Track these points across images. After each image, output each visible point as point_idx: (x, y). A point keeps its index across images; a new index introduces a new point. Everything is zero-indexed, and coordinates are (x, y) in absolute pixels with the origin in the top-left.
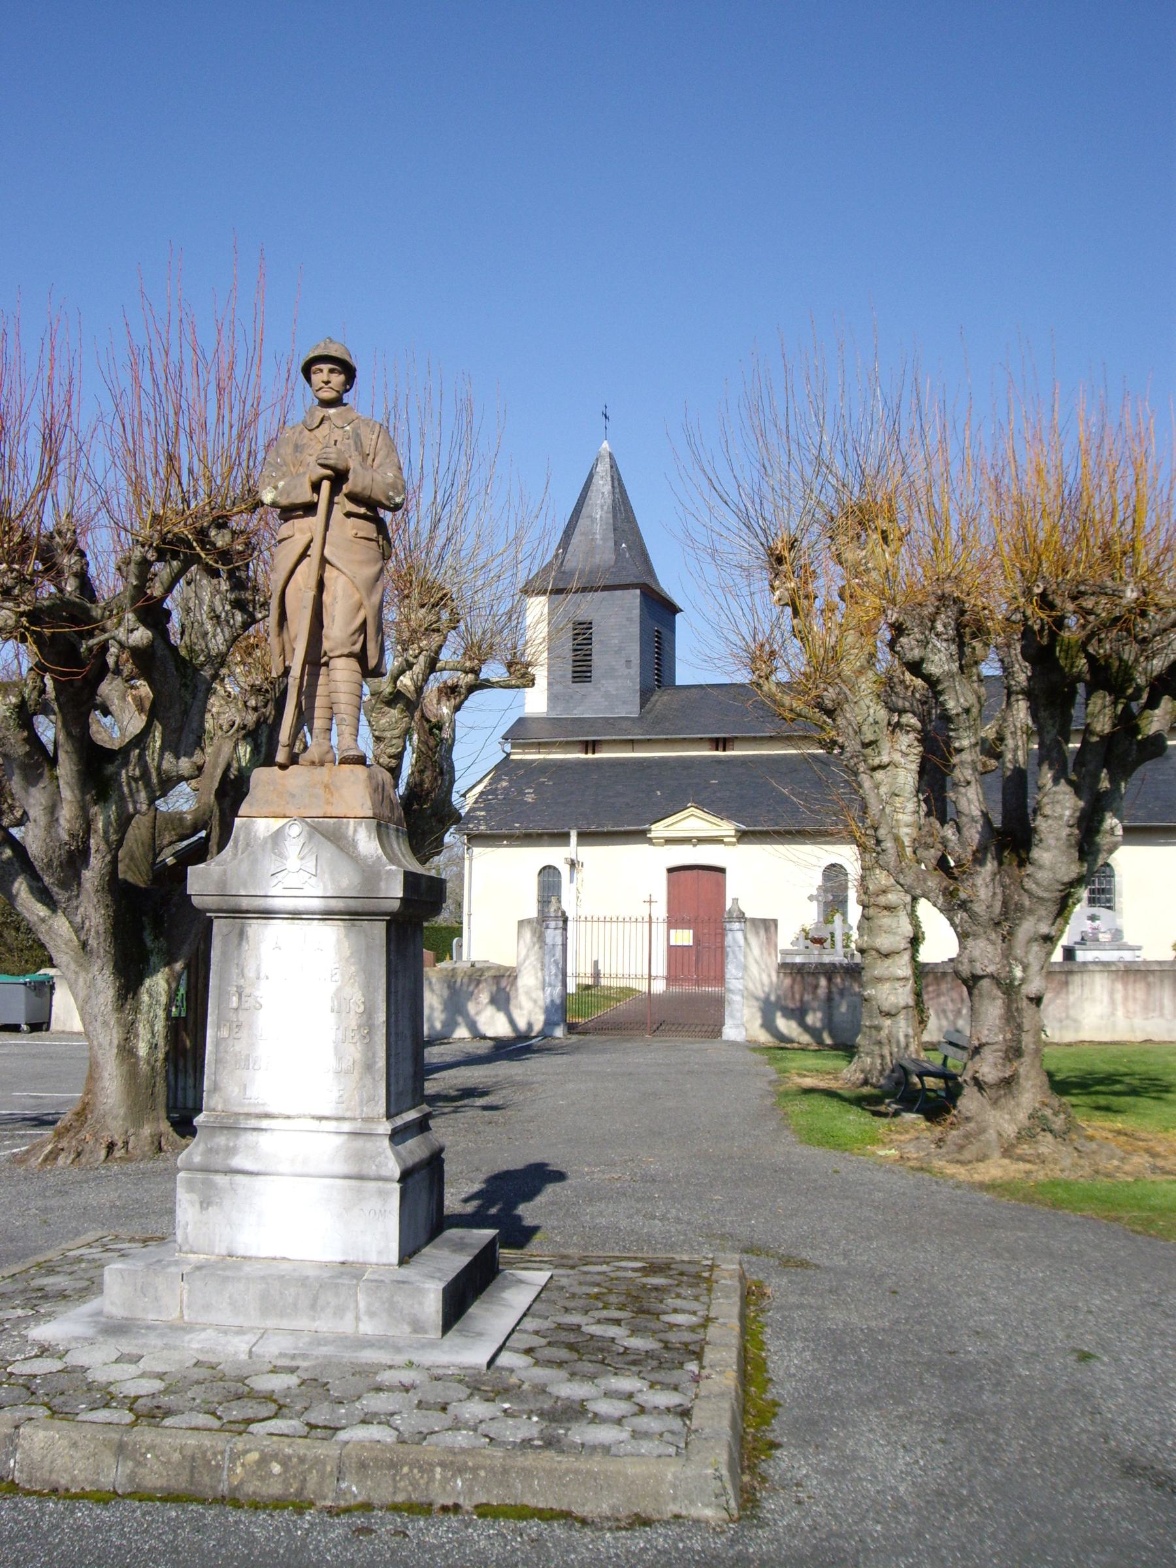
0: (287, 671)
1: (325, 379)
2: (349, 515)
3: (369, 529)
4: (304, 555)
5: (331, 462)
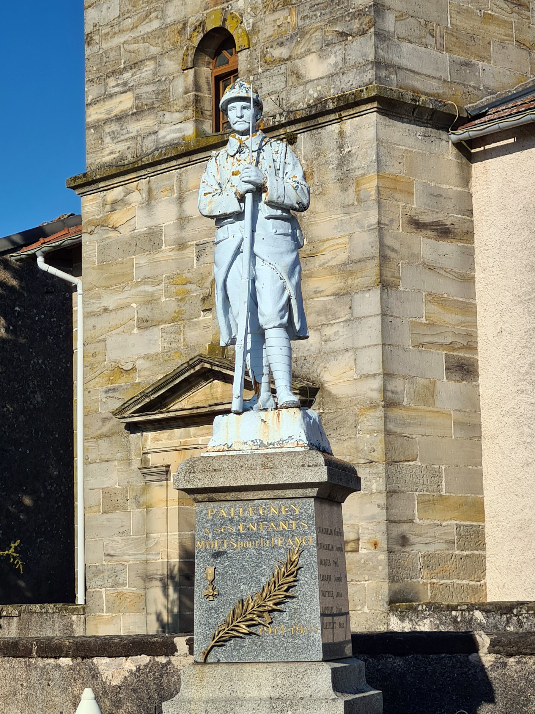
0: (233, 341)
1: (239, 115)
2: (268, 218)
3: (286, 227)
4: (238, 251)
5: (252, 179)
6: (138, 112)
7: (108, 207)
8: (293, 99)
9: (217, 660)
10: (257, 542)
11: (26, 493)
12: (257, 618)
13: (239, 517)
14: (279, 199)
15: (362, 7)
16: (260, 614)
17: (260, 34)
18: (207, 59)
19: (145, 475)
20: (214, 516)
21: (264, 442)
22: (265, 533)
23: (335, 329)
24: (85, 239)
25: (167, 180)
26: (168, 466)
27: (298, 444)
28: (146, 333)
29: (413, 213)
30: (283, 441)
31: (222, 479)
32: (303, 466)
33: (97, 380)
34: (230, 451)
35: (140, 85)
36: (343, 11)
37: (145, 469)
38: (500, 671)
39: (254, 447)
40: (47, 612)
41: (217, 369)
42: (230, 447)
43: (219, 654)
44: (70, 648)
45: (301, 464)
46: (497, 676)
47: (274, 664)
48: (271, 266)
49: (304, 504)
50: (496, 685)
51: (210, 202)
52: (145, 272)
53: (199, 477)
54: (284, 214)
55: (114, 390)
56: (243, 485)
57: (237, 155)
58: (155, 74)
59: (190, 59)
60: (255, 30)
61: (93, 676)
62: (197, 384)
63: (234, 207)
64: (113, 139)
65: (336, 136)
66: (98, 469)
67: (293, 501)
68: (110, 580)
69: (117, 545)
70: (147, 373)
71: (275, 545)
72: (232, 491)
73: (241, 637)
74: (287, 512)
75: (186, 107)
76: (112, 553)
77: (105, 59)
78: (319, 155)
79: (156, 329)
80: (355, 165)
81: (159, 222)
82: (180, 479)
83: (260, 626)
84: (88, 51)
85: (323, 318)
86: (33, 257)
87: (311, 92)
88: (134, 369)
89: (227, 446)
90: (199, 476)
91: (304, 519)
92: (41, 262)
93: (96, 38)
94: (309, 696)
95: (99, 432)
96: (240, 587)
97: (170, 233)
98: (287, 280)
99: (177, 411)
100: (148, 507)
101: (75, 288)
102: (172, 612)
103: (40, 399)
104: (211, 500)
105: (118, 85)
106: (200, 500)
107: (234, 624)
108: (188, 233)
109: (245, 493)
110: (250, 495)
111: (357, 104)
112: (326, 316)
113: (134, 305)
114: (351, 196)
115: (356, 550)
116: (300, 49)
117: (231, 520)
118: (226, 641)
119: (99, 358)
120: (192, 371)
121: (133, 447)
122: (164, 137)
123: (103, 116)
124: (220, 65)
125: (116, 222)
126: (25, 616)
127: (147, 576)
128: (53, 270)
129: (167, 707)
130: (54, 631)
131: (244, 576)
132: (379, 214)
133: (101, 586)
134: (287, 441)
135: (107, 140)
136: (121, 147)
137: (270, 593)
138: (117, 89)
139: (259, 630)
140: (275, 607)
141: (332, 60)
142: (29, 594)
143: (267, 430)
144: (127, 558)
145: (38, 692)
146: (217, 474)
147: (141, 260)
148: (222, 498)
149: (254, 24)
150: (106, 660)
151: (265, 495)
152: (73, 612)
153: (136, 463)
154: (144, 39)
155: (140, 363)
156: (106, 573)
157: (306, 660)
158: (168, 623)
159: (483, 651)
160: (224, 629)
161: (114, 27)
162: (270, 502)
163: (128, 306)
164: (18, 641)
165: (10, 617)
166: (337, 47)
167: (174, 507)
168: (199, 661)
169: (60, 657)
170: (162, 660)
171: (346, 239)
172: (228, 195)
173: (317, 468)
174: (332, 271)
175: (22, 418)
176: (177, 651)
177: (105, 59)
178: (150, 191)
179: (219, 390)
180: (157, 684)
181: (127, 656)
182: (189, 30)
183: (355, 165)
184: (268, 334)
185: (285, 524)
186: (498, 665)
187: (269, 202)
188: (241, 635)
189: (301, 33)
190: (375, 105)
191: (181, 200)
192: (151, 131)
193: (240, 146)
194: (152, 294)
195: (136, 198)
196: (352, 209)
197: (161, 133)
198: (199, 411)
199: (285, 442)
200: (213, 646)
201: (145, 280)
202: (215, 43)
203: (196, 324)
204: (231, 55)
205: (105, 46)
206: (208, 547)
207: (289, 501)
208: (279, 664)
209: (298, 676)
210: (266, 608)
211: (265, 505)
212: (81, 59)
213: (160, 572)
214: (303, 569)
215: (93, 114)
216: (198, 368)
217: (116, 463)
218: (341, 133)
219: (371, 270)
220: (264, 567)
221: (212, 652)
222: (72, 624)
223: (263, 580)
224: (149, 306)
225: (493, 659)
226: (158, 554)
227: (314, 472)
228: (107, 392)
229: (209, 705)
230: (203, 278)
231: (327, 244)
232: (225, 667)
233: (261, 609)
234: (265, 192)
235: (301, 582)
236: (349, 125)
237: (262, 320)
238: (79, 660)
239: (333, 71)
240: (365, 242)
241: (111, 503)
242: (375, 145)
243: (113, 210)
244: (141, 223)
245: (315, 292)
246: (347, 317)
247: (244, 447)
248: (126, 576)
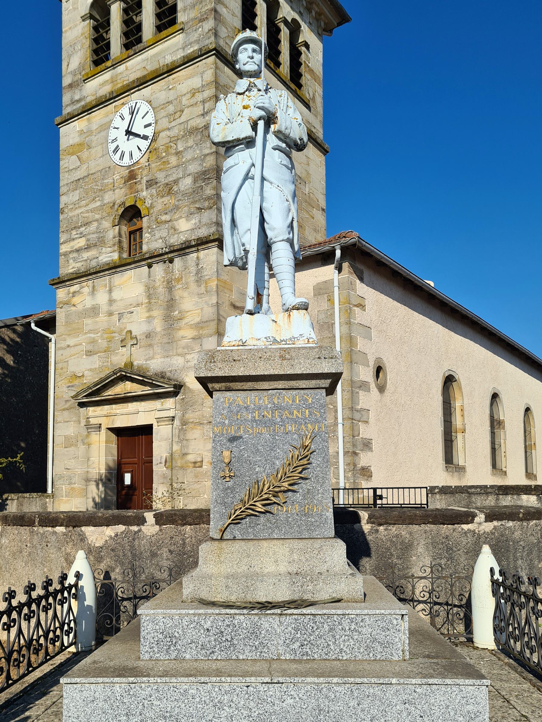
2: (275, 149)
4: (247, 177)
5: (266, 105)
6: (88, 248)
7: (71, 295)
8: (172, 241)
9: (232, 537)
10: (272, 428)
11: (22, 441)
12: (272, 498)
14: (287, 131)
15: (210, 195)
16: (275, 494)
17: (155, 209)
18: (125, 222)
19: (87, 428)
20: (231, 404)
21: (276, 339)
22: (279, 420)
23: (192, 355)
24: (58, 310)
25: (102, 281)
26: (101, 424)
27: (308, 341)
28: (90, 357)
29: (233, 301)
30: (294, 338)
31: (242, 369)
32: (319, 358)
33: (63, 381)
35: (89, 234)
36: (199, 197)
37: (88, 426)
38: (374, 535)
39: (268, 343)
40: (33, 497)
41: (129, 375)
43: (236, 531)
44: (64, 520)
46: (372, 539)
47: (289, 541)
48: (279, 188)
49: (317, 395)
50: (372, 545)
51: (224, 129)
52: (90, 327)
54: (287, 149)
55: (72, 386)
57: (247, 93)
58: (97, 228)
59: (117, 221)
60: (152, 206)
61: (81, 540)
62: (117, 383)
63: (247, 131)
64: (74, 261)
65: (195, 259)
66: (63, 426)
67: (306, 391)
68: (67, 481)
69: (72, 464)
70: (91, 378)
71: (289, 431)
72: (250, 381)
73: (256, 516)
74: (299, 401)
75: (114, 245)
76: (69, 468)
77: (70, 221)
78: (185, 269)
79: (95, 356)
80: (205, 273)
81: (98, 302)
83: (274, 505)
84: (61, 217)
85: (186, 350)
86: (29, 323)
87: (181, 237)
88: (83, 376)
91: (316, 408)
92: (33, 326)
93: (66, 210)
94: (325, 571)
95: (63, 407)
96: (255, 469)
97: (104, 308)
98: (291, 203)
99: (106, 396)
100: (89, 445)
101: (51, 340)
102: (101, 497)
103: (30, 397)
104: (228, 390)
105: (77, 234)
106: (218, 389)
107: (250, 503)
108: (114, 308)
109: (261, 383)
110: (265, 385)
111: (207, 242)
112: (188, 349)
113: (84, 344)
114: (203, 289)
115: (201, 467)
116: (176, 216)
118: (242, 519)
119: (65, 370)
120: (115, 376)
121: (81, 415)
122: (102, 260)
123: (69, 250)
124: (132, 226)
125: (75, 304)
126: (21, 499)
127: (87, 479)
128: (39, 330)
129: (187, 583)
130: (36, 506)
131: (259, 459)
132: (218, 298)
133: (63, 485)
135: (71, 261)
136: (79, 265)
137: (285, 475)
138: (76, 236)
139: (274, 509)
140: (290, 488)
141: (193, 221)
142: (23, 489)
143: (279, 329)
144: (77, 470)
145: (39, 551)
146: (237, 364)
147: (88, 321)
148: (239, 388)
149: (151, 204)
150: (91, 528)
152: (47, 497)
153: (83, 423)
154: (92, 211)
155: (86, 373)
156: (65, 478)
157: (319, 536)
158: (98, 503)
159: (364, 522)
160: (241, 508)
161: (76, 205)
162: (284, 392)
163: (81, 344)
164: (24, 515)
165: (12, 500)
166: (196, 215)
167: (103, 445)
168: (215, 537)
169: (56, 526)
170: (135, 528)
171: (200, 311)
172: (241, 121)
173: (333, 360)
174: (191, 327)
175: (20, 405)
176: (146, 522)
177: (70, 221)
178: (94, 287)
179: (129, 386)
180: (130, 546)
181: (108, 526)
182: (116, 206)
183: (205, 273)
184: (274, 247)
185: (298, 412)
186: (373, 531)
188: (257, 513)
189: (177, 208)
190: (217, 243)
191: (110, 291)
192: (95, 257)
193: (249, 85)
194: (94, 338)
195: (86, 290)
196: (203, 295)
197: (100, 258)
198: (118, 396)
199: (296, 339)
200: (230, 524)
201: (90, 331)
202: (130, 214)
203: (117, 353)
204: (138, 221)
205: (71, 214)
206: (225, 432)
207: (302, 391)
208: (294, 540)
209: (314, 552)
210: (282, 488)
212: (58, 221)
213: (95, 477)
214: (315, 453)
215: (63, 249)
216: (118, 375)
217: (72, 423)
218: (198, 258)
219: (213, 326)
220: (279, 451)
221: (228, 529)
222: (46, 504)
223: (277, 463)
224: (92, 345)
225: (370, 528)
226: (94, 468)
227: (330, 364)
228: (68, 387)
229: (230, 581)
230: (122, 330)
231: (189, 313)
232: (243, 543)
233: (277, 489)
234: (274, 123)
235: (314, 465)
236: (202, 254)
237: (270, 234)
238: (71, 528)
239: (194, 227)
240: (209, 312)
241: (69, 442)
242: (216, 264)
243: (73, 296)
244: (89, 302)
245: (182, 337)
246: (199, 350)
247: (258, 343)
248: (76, 479)
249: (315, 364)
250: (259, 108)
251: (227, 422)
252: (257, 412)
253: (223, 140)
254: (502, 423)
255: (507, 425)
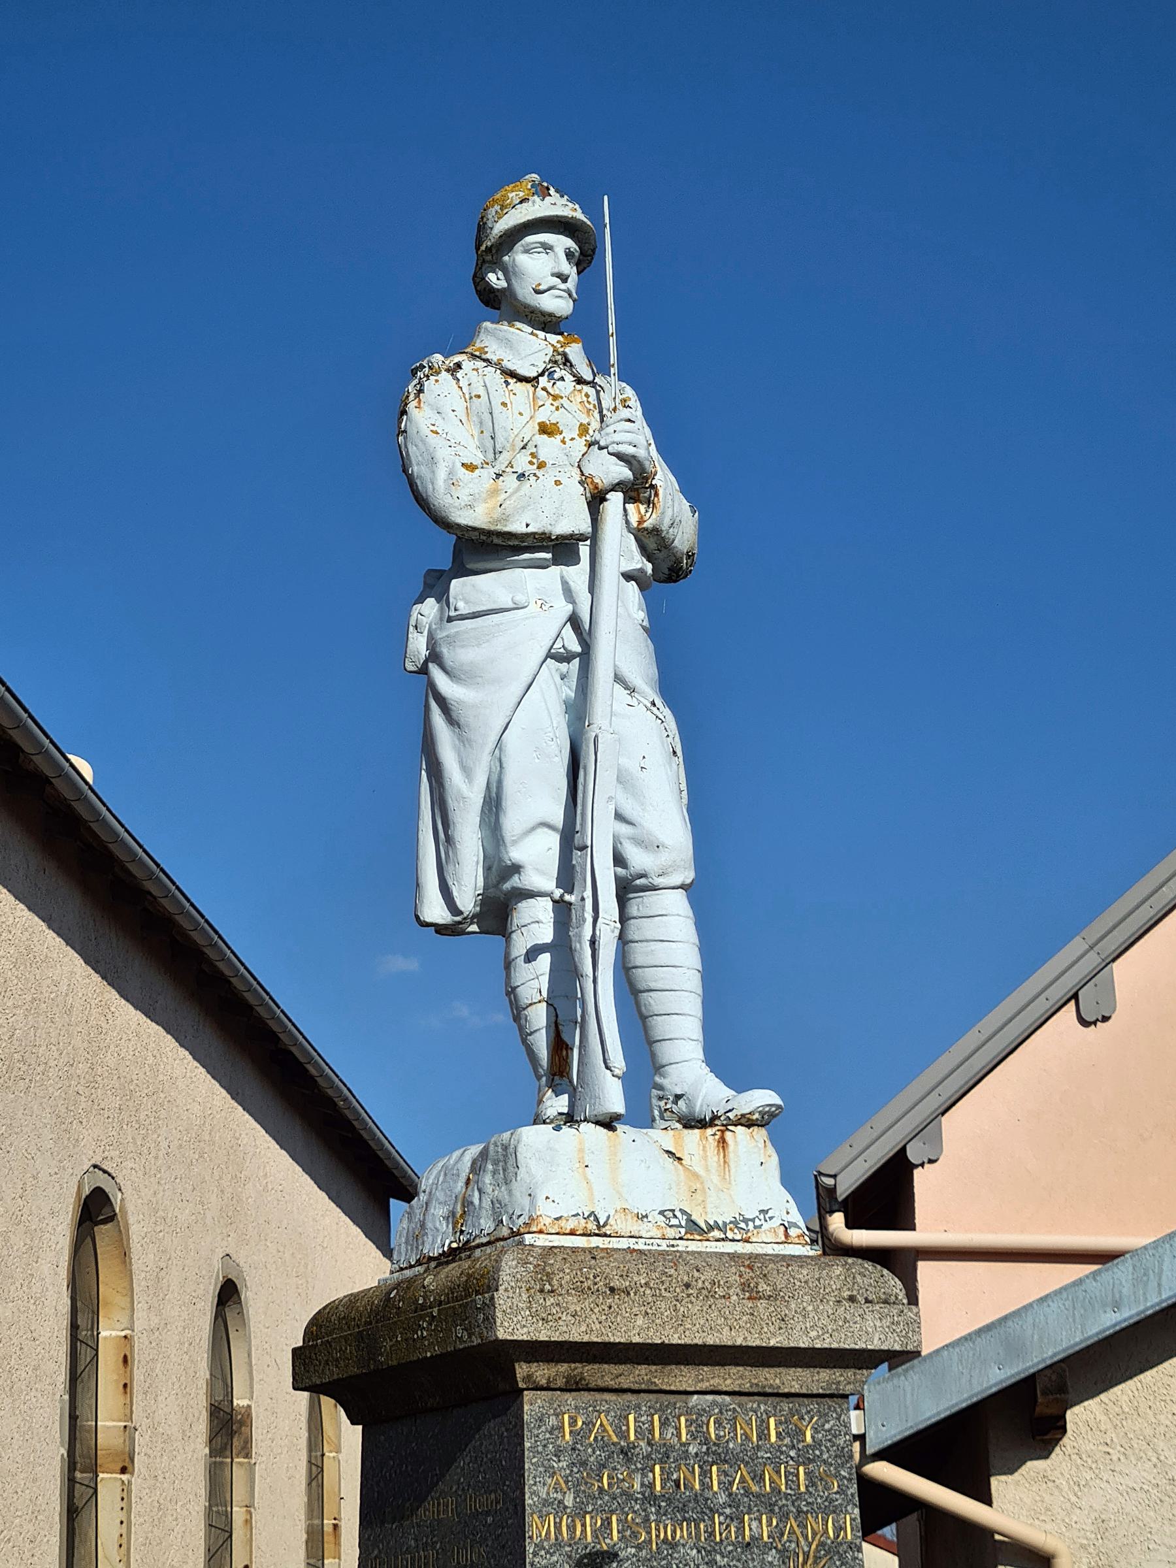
2: (628, 576)
13: (649, 1444)
22: (722, 1498)
27: (787, 1235)
30: (746, 1221)
31: (640, 1321)
32: (852, 1299)
34: (605, 1235)
39: (671, 1233)
42: (604, 1226)
45: (846, 1294)
48: (655, 709)
53: (572, 1308)
56: (700, 1342)
63: (572, 518)
74: (779, 1435)
82: (519, 1310)
89: (597, 1220)
90: (573, 1302)
91: (825, 1462)
104: (574, 1386)
106: (544, 1382)
117: (627, 1453)
134: (757, 1223)
146: (626, 1306)
151: (728, 1382)
172: (558, 483)
187: (655, 531)
211: (721, 1412)
247: (643, 1229)
249: (845, 1321)
250: (620, 456)
251: (569, 1501)
252: (657, 1468)
253: (493, 528)
254: (242, 1423)
255: (259, 1433)
